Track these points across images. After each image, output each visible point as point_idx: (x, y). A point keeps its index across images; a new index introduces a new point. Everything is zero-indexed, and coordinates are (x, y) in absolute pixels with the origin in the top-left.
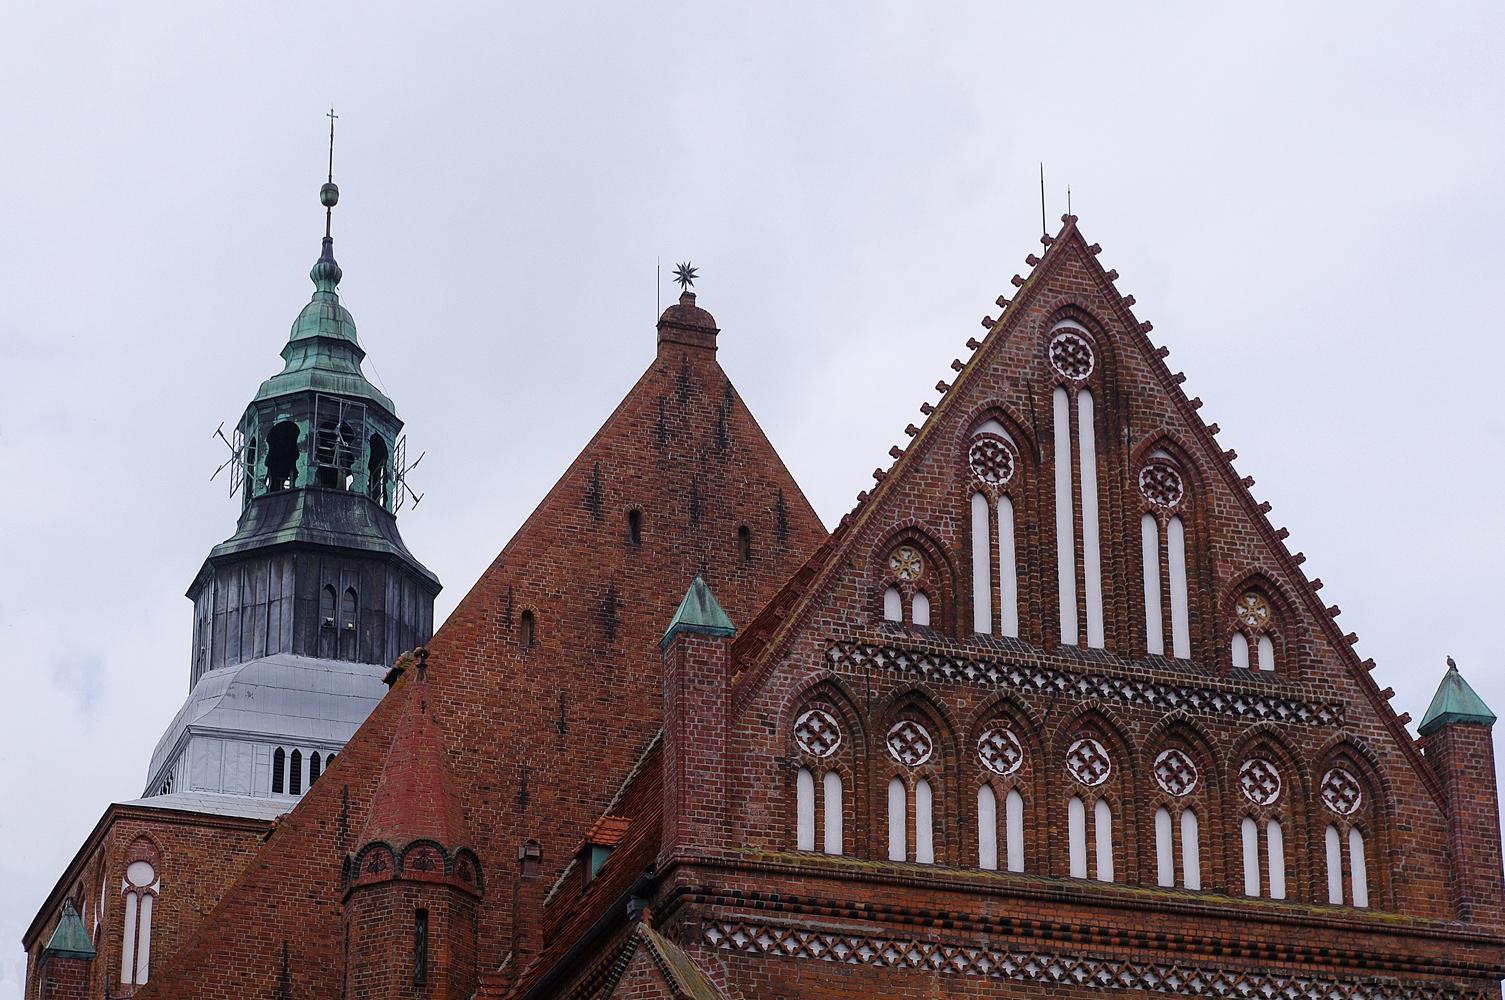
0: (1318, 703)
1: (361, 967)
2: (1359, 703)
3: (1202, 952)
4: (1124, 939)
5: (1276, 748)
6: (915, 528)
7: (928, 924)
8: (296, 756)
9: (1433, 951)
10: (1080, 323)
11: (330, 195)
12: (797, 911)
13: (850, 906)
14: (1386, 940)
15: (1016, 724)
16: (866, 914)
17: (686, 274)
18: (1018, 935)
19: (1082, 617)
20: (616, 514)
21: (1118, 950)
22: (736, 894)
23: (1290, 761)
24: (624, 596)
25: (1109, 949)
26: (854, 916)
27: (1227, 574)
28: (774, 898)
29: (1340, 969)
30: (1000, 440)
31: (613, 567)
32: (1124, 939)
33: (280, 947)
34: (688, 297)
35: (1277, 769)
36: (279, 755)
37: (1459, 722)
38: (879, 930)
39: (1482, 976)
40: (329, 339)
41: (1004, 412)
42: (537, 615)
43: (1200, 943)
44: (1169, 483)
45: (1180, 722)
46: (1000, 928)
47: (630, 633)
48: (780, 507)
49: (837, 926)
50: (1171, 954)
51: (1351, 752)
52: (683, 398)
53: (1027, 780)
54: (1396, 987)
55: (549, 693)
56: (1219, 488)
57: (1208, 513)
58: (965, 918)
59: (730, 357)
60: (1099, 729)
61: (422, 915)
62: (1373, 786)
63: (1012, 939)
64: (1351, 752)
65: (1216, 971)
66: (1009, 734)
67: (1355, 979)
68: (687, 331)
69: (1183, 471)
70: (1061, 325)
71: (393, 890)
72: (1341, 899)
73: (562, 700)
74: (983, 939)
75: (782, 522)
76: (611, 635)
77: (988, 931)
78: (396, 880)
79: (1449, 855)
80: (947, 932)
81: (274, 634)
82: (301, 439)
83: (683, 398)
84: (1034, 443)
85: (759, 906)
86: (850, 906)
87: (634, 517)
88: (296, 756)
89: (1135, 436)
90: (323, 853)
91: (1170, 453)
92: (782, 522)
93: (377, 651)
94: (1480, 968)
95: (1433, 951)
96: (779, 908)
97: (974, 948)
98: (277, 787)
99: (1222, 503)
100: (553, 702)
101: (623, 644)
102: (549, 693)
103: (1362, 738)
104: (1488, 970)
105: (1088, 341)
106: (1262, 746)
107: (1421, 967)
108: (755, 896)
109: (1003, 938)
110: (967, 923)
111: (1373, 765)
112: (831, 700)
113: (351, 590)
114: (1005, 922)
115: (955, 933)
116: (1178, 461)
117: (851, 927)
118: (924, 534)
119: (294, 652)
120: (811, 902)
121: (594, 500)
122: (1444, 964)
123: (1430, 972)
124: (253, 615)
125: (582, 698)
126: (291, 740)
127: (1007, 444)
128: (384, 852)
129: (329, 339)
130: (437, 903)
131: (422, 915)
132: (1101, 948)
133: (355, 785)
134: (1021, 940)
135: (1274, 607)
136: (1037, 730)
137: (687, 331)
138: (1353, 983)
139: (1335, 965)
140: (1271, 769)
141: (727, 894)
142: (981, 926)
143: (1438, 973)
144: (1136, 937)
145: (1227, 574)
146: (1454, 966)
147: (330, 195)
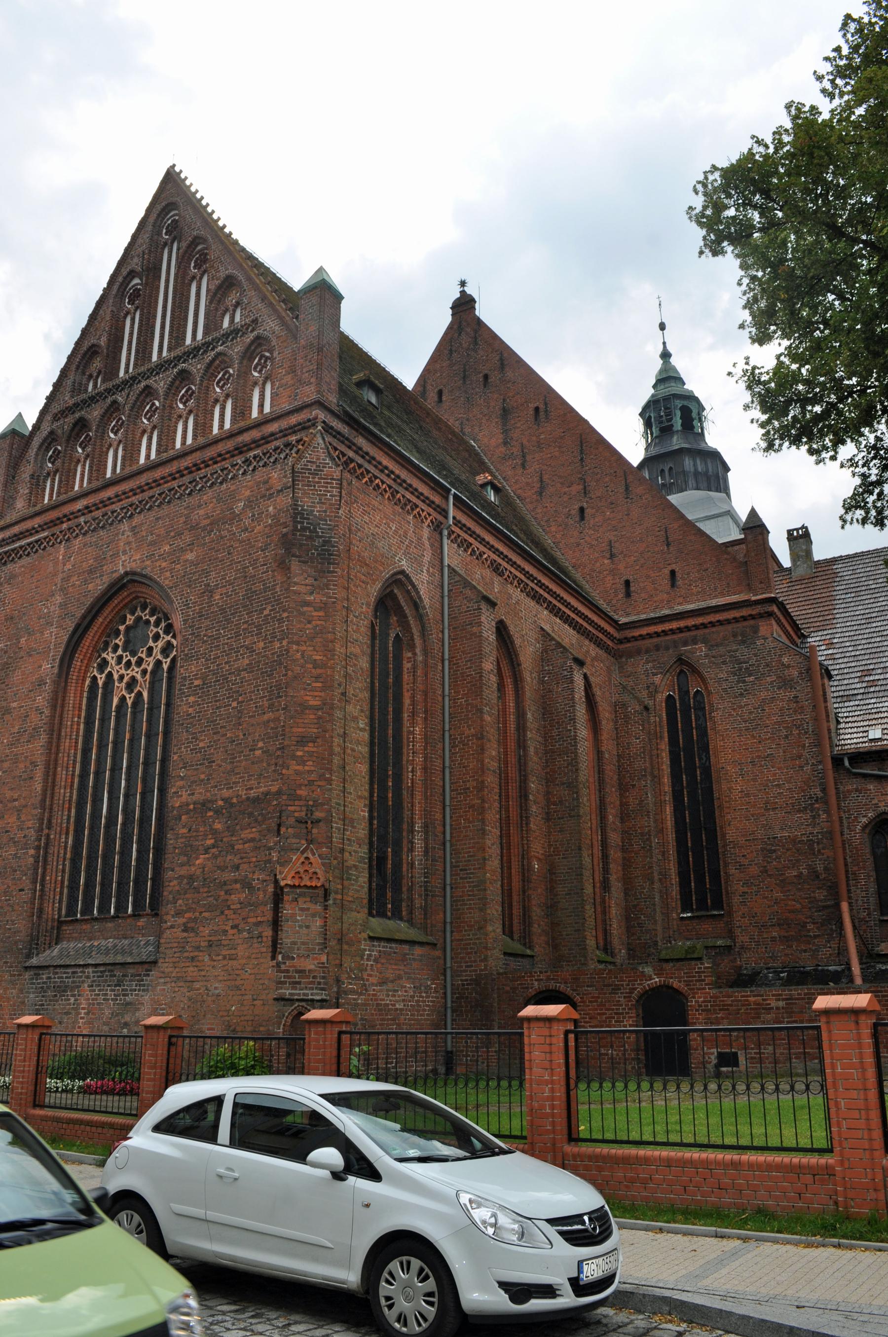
11: (662, 327)
17: (463, 284)
26: (37, 532)
34: (463, 293)
40: (668, 377)
52: (460, 335)
58: (73, 513)
68: (464, 305)
75: (502, 364)
85: (8, 544)
86: (34, 528)
87: (440, 393)
92: (502, 364)
93: (684, 487)
94: (300, 424)
96: (13, 541)
104: (305, 423)
114: (87, 507)
129: (668, 377)
137: (464, 305)
143: (280, 438)
147: (662, 327)
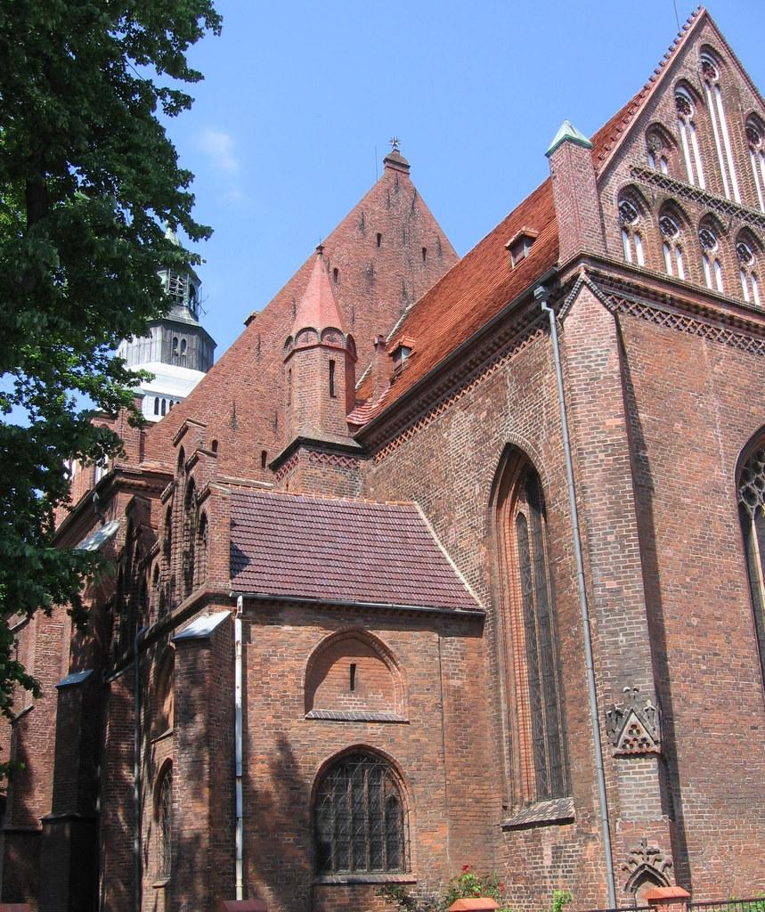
1: (300, 387)
6: (659, 124)
8: (164, 401)
12: (638, 294)
20: (372, 235)
24: (376, 269)
26: (664, 302)
30: (686, 97)
31: (371, 256)
33: (232, 403)
36: (157, 400)
41: (689, 83)
42: (340, 271)
47: (379, 285)
48: (439, 243)
52: (397, 191)
55: (346, 305)
59: (416, 177)
61: (332, 363)
66: (710, 233)
71: (318, 349)
73: (353, 309)
76: (372, 284)
78: (319, 345)
81: (153, 355)
82: (163, 282)
83: (397, 191)
85: (621, 288)
87: (379, 236)
88: (164, 401)
90: (249, 362)
96: (630, 291)
98: (156, 413)
100: (348, 309)
101: (377, 289)
102: (346, 305)
112: (633, 196)
113: (184, 340)
116: (758, 125)
118: (664, 128)
119: (162, 362)
121: (362, 226)
124: (144, 348)
125: (361, 310)
126: (162, 395)
128: (311, 334)
130: (340, 359)
131: (332, 363)
133: (264, 334)
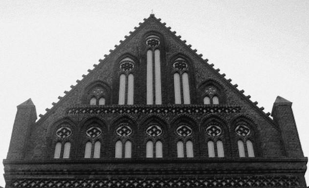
0: (231, 107)
2: (245, 106)
3: (189, 174)
4: (160, 172)
5: (218, 120)
7: (90, 174)
9: (276, 166)
10: (154, 35)
13: (62, 171)
14: (257, 164)
15: (130, 124)
16: (67, 173)
18: (122, 174)
19: (154, 96)
21: (158, 176)
22: (23, 171)
23: (223, 124)
25: (155, 176)
26: (63, 174)
27: (199, 81)
28: (36, 171)
29: (241, 175)
32: (160, 172)
35: (220, 127)
37: (279, 105)
38: (73, 177)
39: (296, 172)
43: (187, 171)
44: (184, 65)
45: (184, 116)
46: (115, 173)
49: (58, 177)
50: (178, 175)
51: (244, 119)
53: (132, 137)
54: (263, 178)
56: (196, 62)
57: (193, 68)
60: (158, 122)
62: (253, 127)
63: (120, 176)
64: (244, 119)
65: (195, 179)
67: (248, 177)
69: (187, 62)
70: (150, 37)
72: (214, 155)
74: (109, 177)
77: (111, 174)
79: (281, 141)
80: (96, 176)
84: (140, 61)
89: (170, 54)
91: (182, 58)
95: (276, 166)
96: (38, 174)
97: (106, 180)
99: (197, 65)
103: (247, 114)
105: (158, 39)
106: (213, 121)
107: (272, 171)
108: (29, 171)
109: (116, 176)
110: (103, 172)
111: (252, 121)
115: (99, 176)
117: (62, 177)
120: (48, 171)
122: (280, 169)
123: (276, 173)
127: (132, 62)
132: (151, 176)
134: (123, 176)
135: (217, 88)
136: (134, 123)
138: (107, 179)
139: (239, 173)
140: (218, 127)
141: (20, 171)
142: (108, 173)
144: (122, 171)
145: (199, 81)
146: (284, 170)
